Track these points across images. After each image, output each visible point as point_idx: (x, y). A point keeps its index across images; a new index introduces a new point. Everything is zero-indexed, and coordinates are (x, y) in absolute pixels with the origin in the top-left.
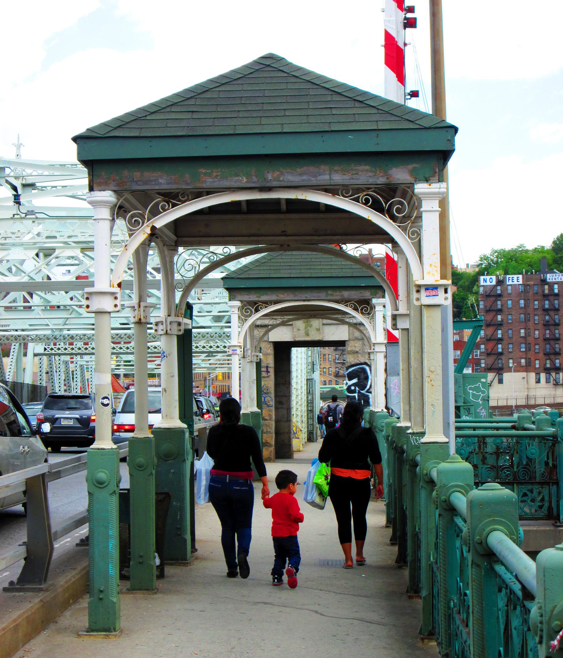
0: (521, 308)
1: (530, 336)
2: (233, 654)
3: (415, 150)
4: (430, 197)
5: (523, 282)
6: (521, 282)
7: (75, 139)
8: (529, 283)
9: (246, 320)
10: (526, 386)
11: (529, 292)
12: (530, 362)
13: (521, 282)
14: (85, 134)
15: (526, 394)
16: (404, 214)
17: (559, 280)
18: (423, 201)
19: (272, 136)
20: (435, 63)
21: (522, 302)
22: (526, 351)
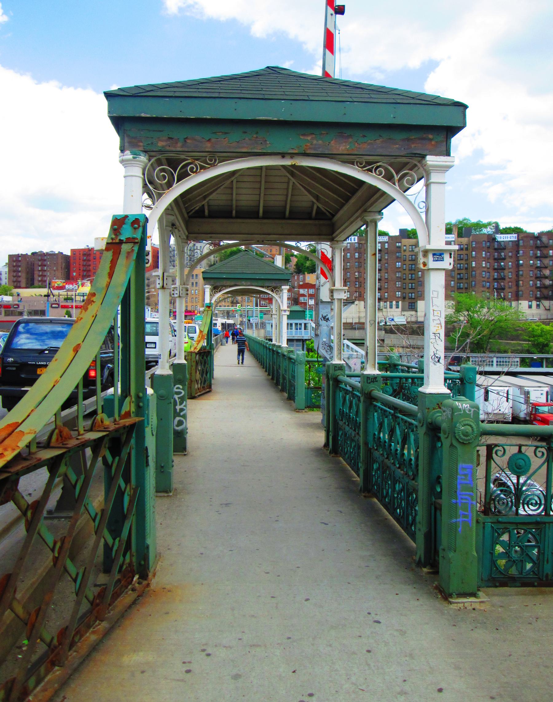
0: (356, 258)
1: (361, 277)
2: (202, 309)
3: (307, 120)
4: (440, 170)
5: (358, 241)
6: (356, 241)
7: (109, 95)
8: (361, 242)
9: (160, 195)
10: (358, 310)
11: (361, 248)
12: (361, 295)
13: (356, 241)
14: (116, 93)
15: (358, 315)
16: (156, 172)
17: (382, 241)
18: (432, 174)
19: (230, 99)
20: (236, 79)
21: (357, 254)
22: (358, 287)
